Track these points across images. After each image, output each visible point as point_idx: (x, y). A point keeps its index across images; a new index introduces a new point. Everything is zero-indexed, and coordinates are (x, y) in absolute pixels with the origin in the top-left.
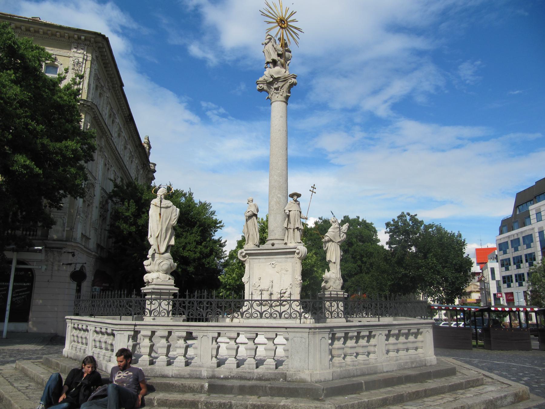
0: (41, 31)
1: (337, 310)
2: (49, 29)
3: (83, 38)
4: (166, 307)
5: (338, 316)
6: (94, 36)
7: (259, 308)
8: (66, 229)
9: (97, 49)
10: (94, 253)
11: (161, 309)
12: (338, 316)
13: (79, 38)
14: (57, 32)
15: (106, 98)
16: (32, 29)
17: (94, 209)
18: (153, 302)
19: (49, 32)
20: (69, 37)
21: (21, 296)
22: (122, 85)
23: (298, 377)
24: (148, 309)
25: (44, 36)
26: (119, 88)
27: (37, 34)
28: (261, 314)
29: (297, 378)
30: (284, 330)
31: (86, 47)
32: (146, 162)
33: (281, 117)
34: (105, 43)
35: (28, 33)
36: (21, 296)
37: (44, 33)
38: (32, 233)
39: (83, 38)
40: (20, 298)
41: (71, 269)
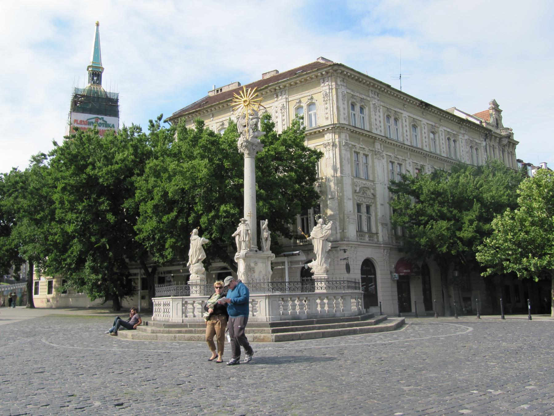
2: (301, 78)
10: (382, 245)
15: (372, 106)
17: (379, 206)
19: (303, 80)
22: (389, 86)
26: (389, 89)
27: (297, 85)
35: (292, 87)
37: (301, 82)
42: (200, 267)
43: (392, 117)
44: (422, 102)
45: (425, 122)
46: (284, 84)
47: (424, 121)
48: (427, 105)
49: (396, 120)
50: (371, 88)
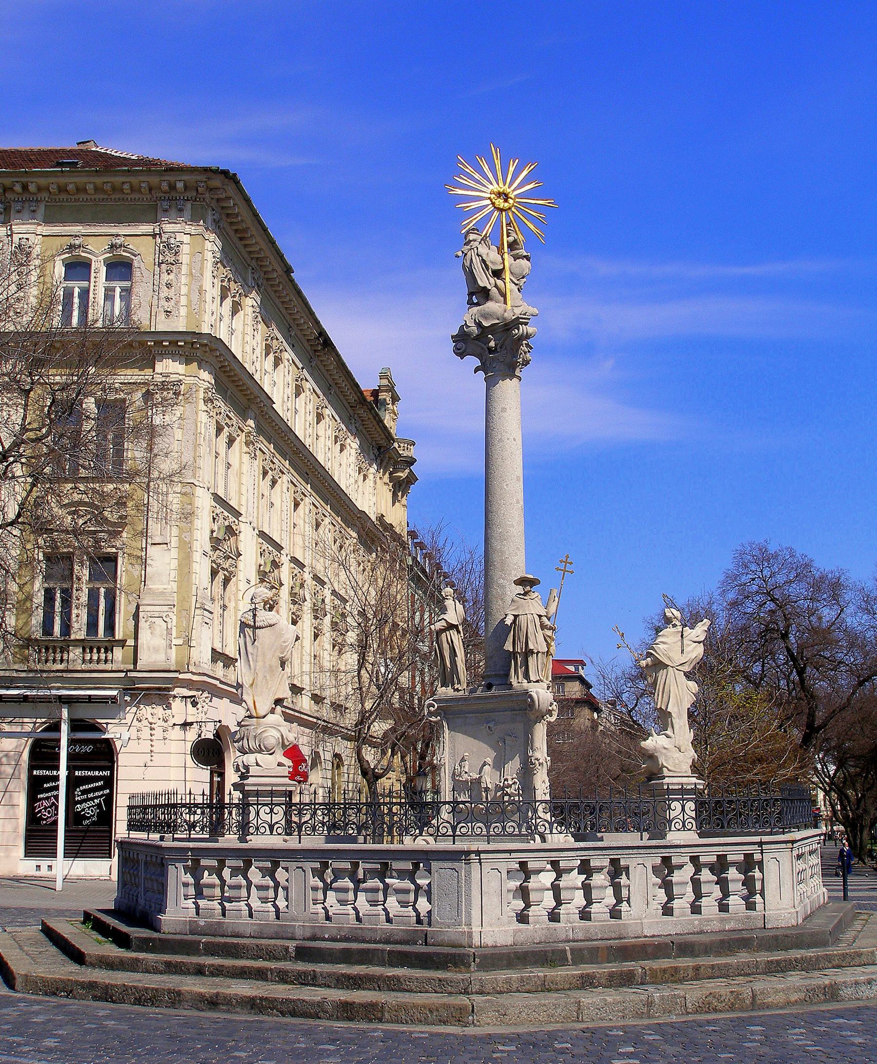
0: (90, 187)
1: (681, 817)
3: (180, 185)
4: (267, 818)
5: (684, 825)
6: (203, 178)
7: (267, 818)
8: (175, 642)
9: (214, 204)
11: (260, 822)
12: (684, 825)
13: (172, 187)
14: (123, 183)
16: (71, 187)
18: (275, 811)
19: (107, 187)
20: (150, 190)
21: (92, 799)
22: (288, 270)
23: (446, 939)
24: (295, 823)
25: (97, 197)
28: (271, 827)
29: (444, 939)
30: (507, 855)
31: (189, 205)
32: (383, 443)
33: (504, 410)
34: (231, 190)
36: (92, 799)
38: (103, 656)
39: (180, 185)
40: (91, 803)
41: (192, 735)
44: (322, 333)
46: (42, 181)
48: (327, 343)
50: (254, 263)
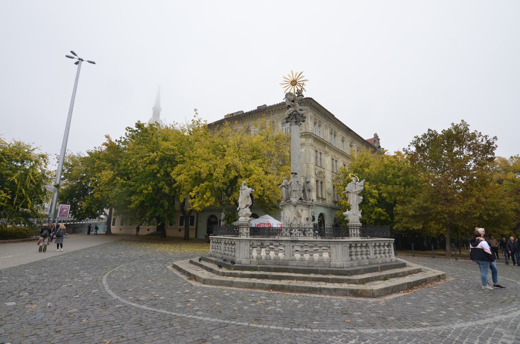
22: (333, 116)
42: (248, 211)
43: (333, 134)
44: (348, 128)
45: (348, 139)
47: (347, 139)
49: (335, 136)
